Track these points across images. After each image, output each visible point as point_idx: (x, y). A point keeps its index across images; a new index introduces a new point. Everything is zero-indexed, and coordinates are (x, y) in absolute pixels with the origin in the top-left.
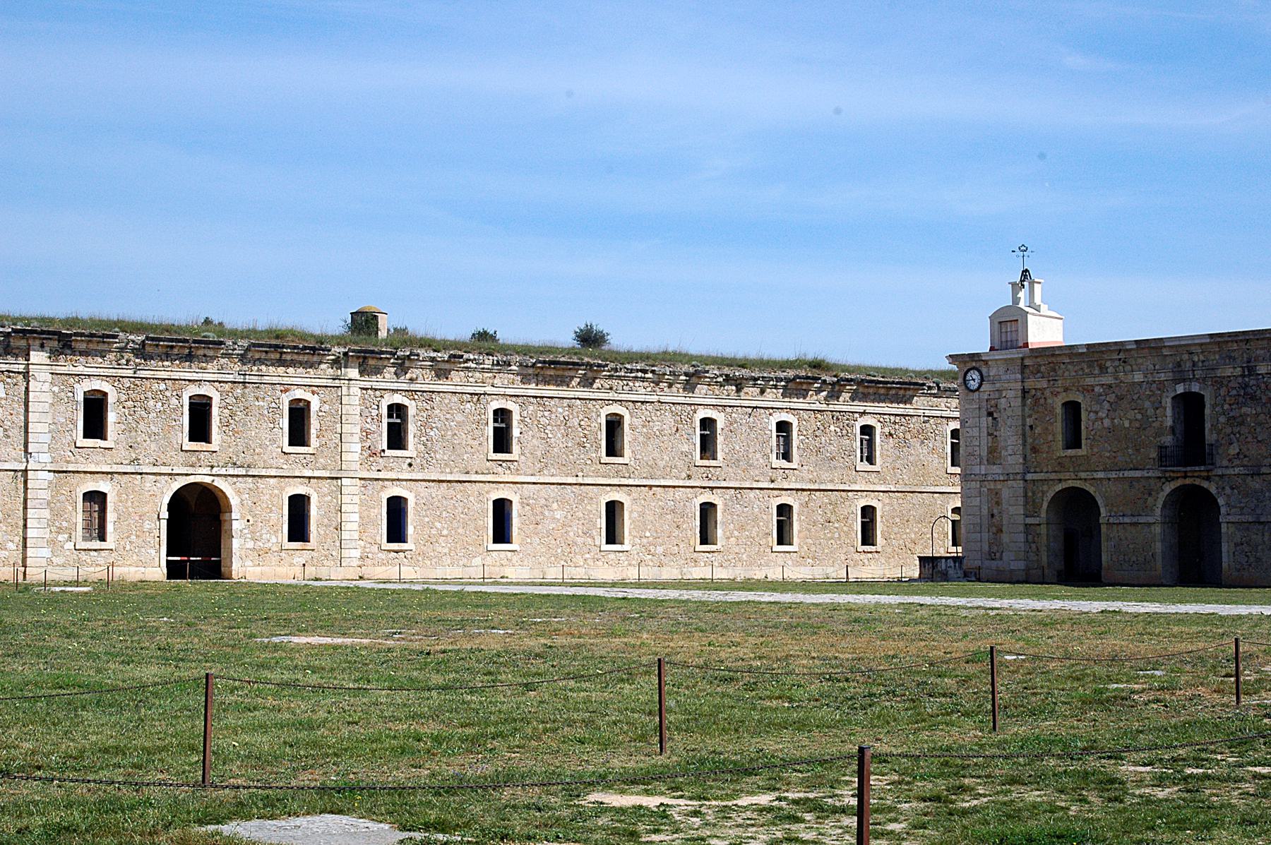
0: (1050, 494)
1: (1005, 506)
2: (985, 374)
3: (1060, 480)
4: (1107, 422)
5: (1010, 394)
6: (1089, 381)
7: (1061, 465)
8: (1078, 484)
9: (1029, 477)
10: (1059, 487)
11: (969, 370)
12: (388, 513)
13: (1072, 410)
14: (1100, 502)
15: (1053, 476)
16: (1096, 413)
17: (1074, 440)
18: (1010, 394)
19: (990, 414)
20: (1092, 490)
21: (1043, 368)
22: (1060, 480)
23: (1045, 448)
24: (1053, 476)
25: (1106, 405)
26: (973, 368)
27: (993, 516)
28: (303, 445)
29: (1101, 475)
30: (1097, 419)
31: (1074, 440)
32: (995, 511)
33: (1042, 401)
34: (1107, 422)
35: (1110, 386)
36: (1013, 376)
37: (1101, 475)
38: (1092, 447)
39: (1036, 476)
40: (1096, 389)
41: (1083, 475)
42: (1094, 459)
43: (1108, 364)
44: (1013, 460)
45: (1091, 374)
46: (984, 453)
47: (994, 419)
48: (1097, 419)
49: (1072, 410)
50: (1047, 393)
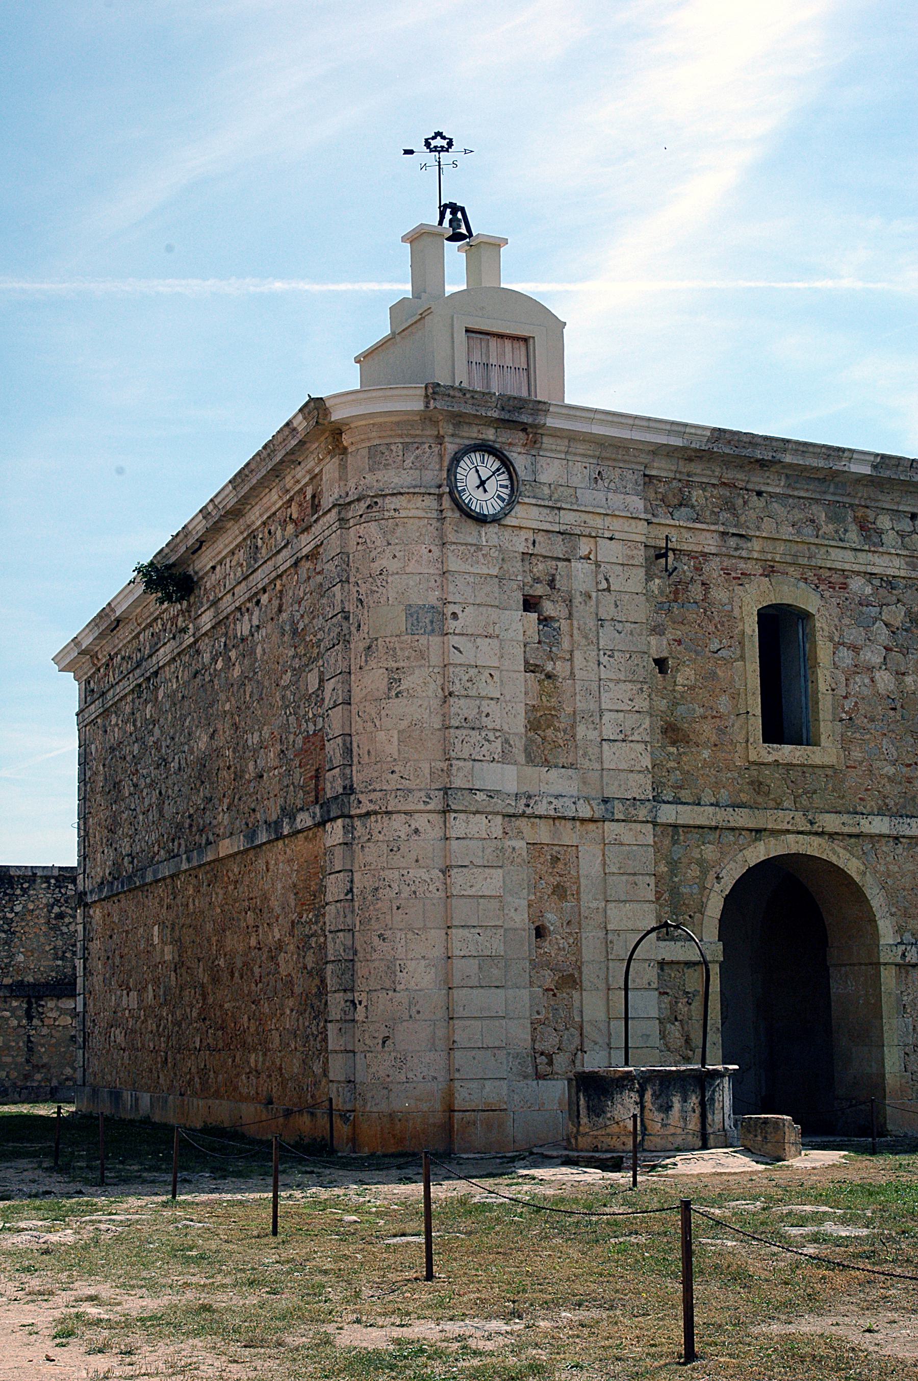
0: (732, 873)
1: (590, 901)
2: (522, 473)
3: (758, 832)
4: (885, 681)
5: (609, 552)
6: (841, 559)
7: (757, 788)
8: (813, 847)
9: (668, 814)
10: (758, 853)
11: (456, 460)
12: (760, 657)
13: (781, 631)
14: (877, 900)
15: (742, 818)
16: (855, 649)
17: (783, 718)
18: (609, 552)
19: (530, 604)
20: (852, 866)
21: (697, 495)
22: (758, 832)
23: (707, 730)
24: (742, 818)
25: (883, 635)
26: (485, 448)
27: (540, 932)
28: (797, 741)
29: (880, 825)
30: (857, 669)
31: (783, 718)
32: (551, 918)
33: (696, 591)
34: (885, 681)
35: (889, 583)
36: (616, 500)
37: (880, 825)
38: (846, 744)
39: (686, 815)
40: (857, 584)
41: (831, 822)
42: (852, 779)
43: (884, 522)
44: (627, 763)
45: (841, 543)
46: (518, 724)
47: (544, 621)
48: (857, 669)
49: (781, 631)
50: (713, 568)
